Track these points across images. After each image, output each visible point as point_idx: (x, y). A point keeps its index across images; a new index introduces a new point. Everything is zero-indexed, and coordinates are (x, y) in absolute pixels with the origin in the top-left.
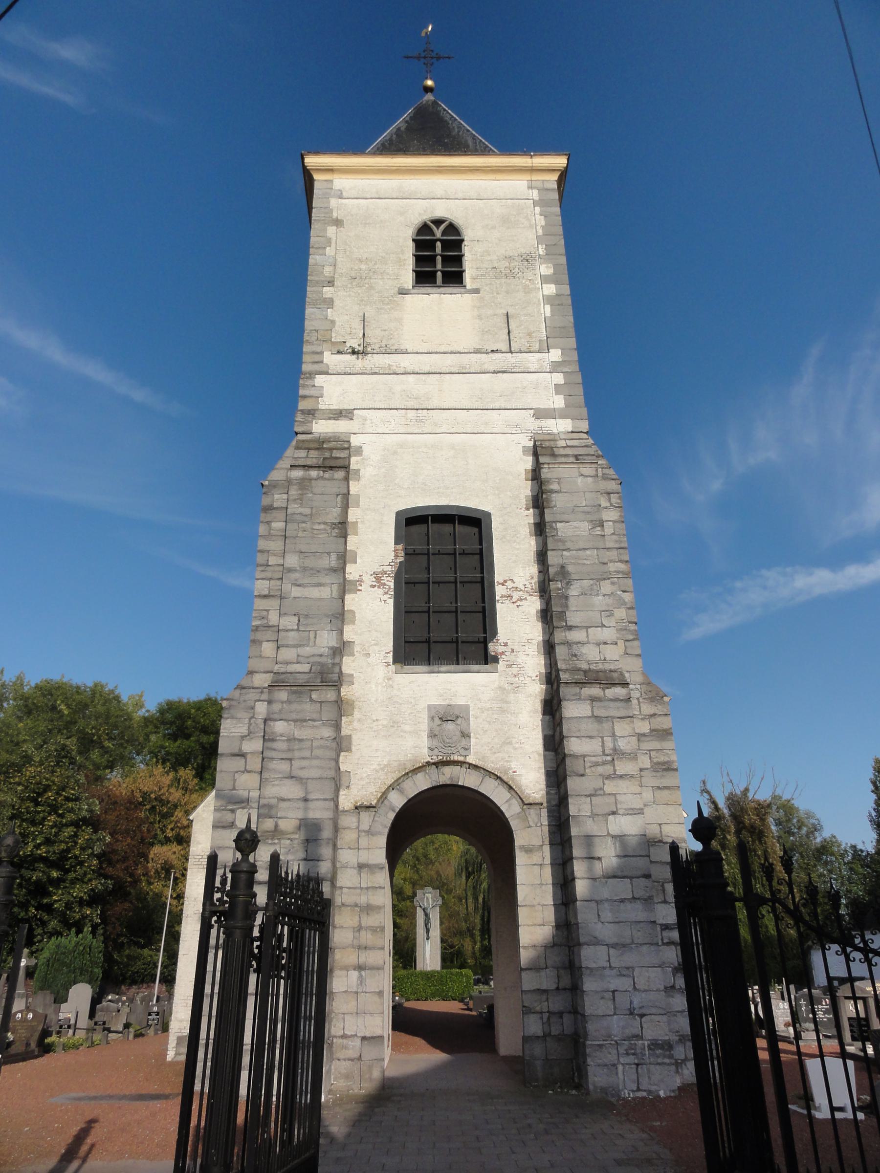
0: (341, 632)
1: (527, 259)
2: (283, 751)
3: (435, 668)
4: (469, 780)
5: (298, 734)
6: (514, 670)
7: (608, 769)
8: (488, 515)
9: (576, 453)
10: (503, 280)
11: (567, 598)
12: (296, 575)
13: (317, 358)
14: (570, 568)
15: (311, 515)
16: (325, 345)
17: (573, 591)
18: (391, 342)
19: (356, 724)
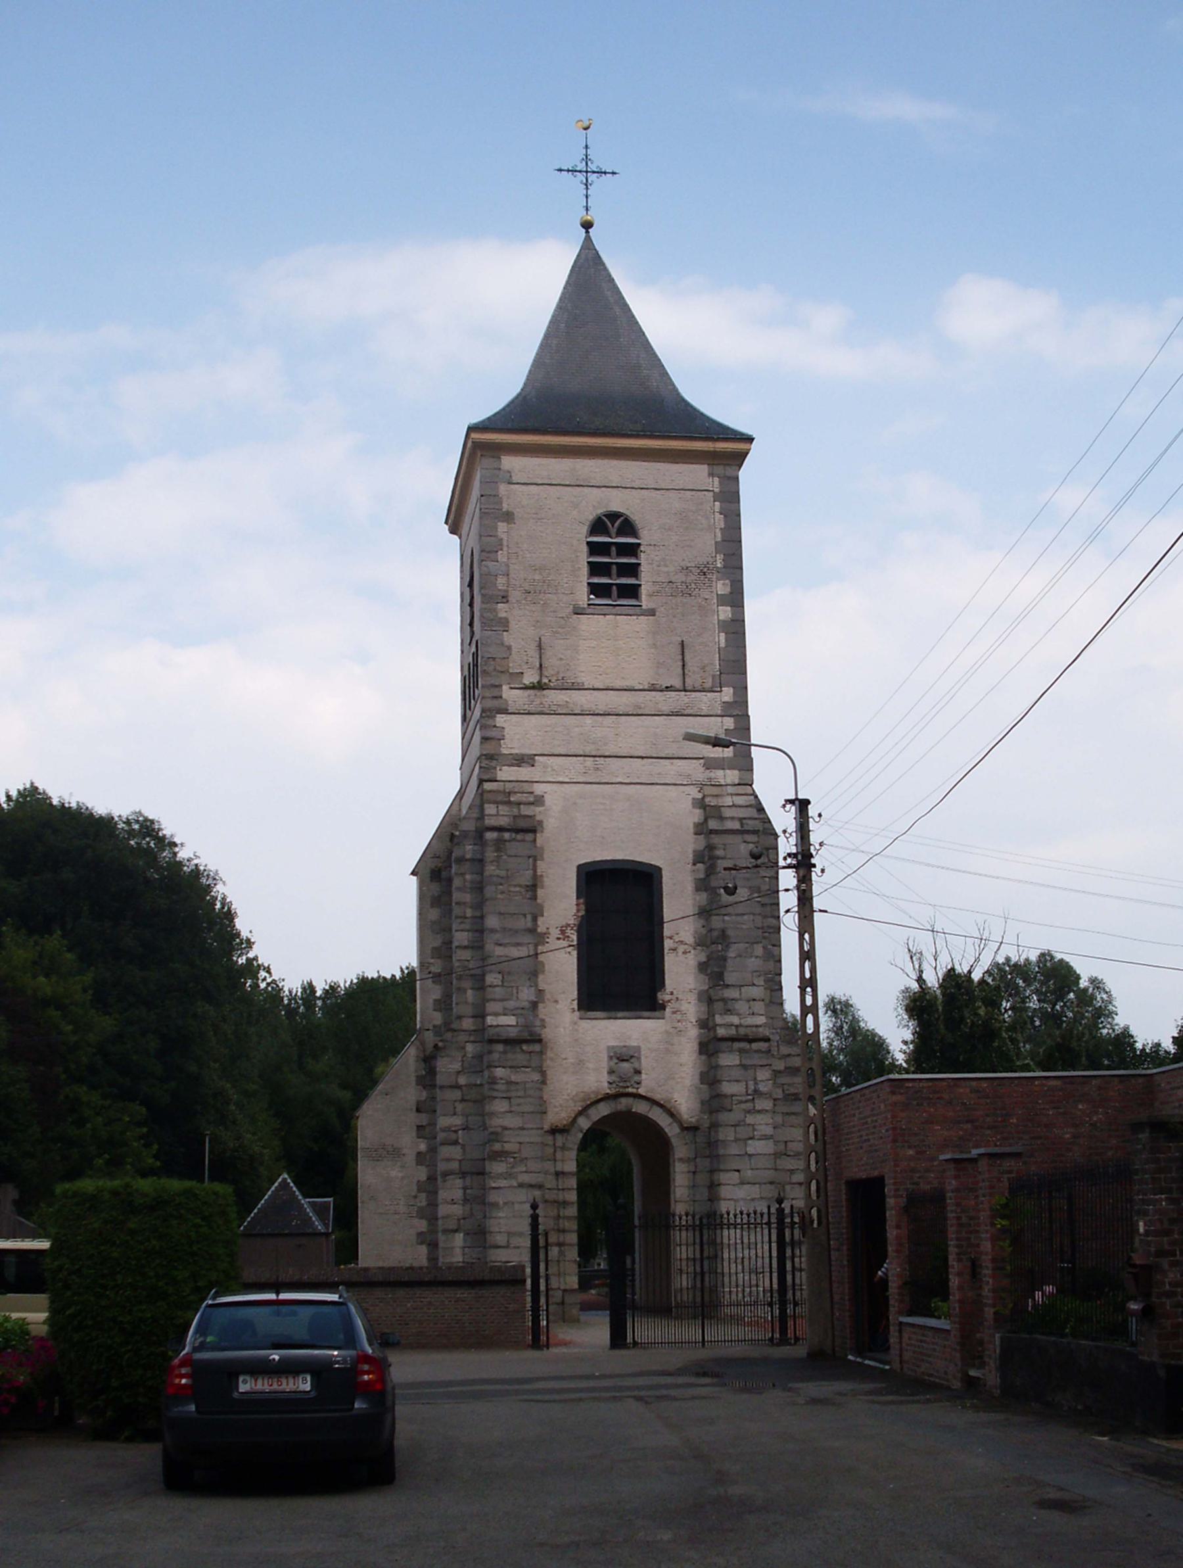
0: (536, 986)
1: (704, 571)
2: (503, 1092)
3: (613, 1014)
4: (641, 1108)
5: (513, 1078)
6: (679, 1017)
7: (749, 1105)
8: (659, 869)
9: (741, 816)
10: (679, 599)
11: (725, 959)
12: (497, 936)
13: (495, 692)
14: (730, 933)
15: (508, 877)
16: (504, 678)
17: (731, 954)
18: (568, 674)
19: (548, 1062)
